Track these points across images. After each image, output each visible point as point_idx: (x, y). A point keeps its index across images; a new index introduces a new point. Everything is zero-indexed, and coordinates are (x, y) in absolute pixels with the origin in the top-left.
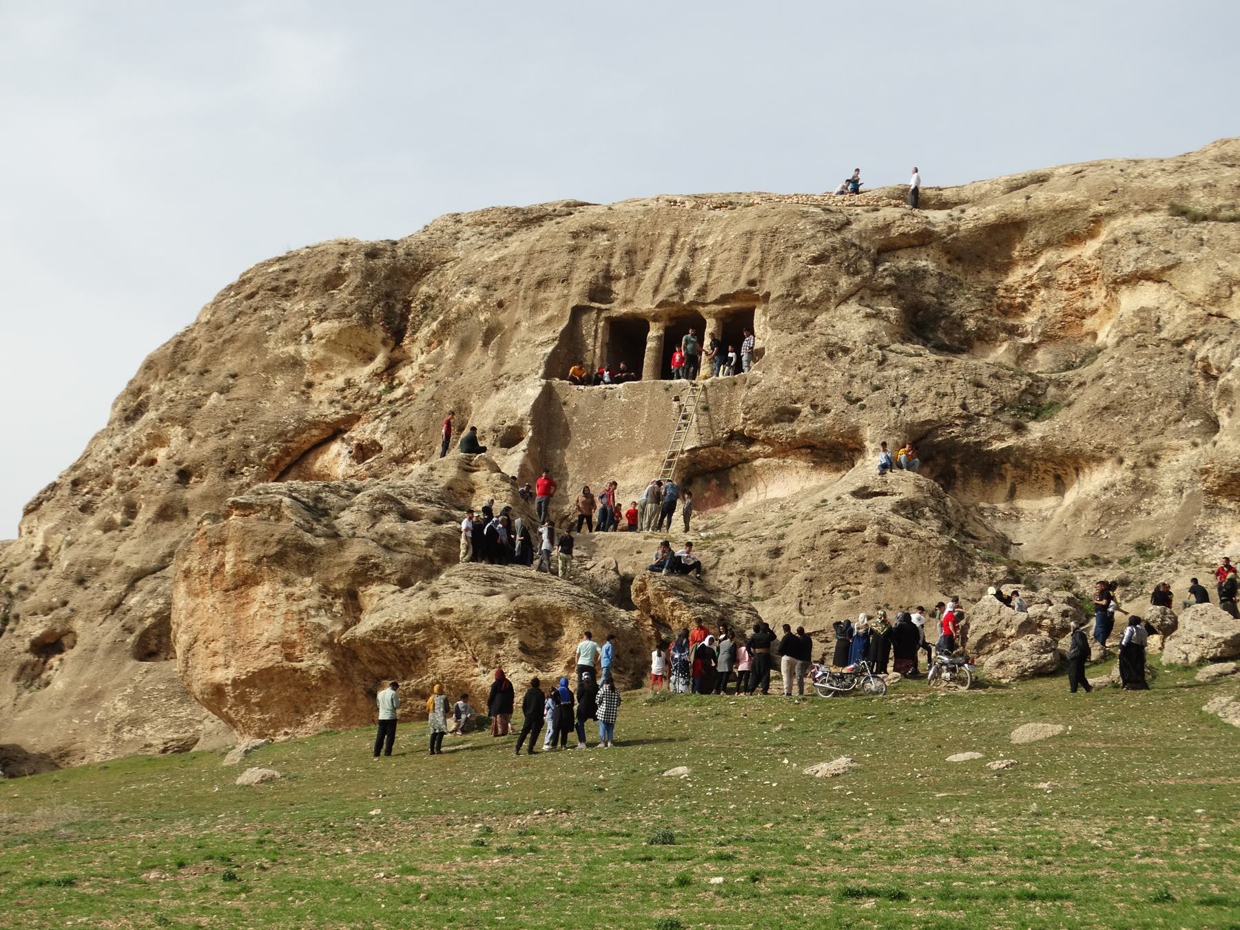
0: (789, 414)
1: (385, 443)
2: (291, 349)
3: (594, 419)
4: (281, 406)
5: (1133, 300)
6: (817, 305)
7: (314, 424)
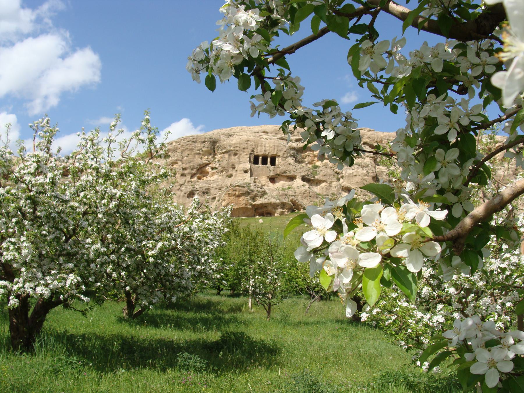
0: (285, 172)
6: (286, 157)
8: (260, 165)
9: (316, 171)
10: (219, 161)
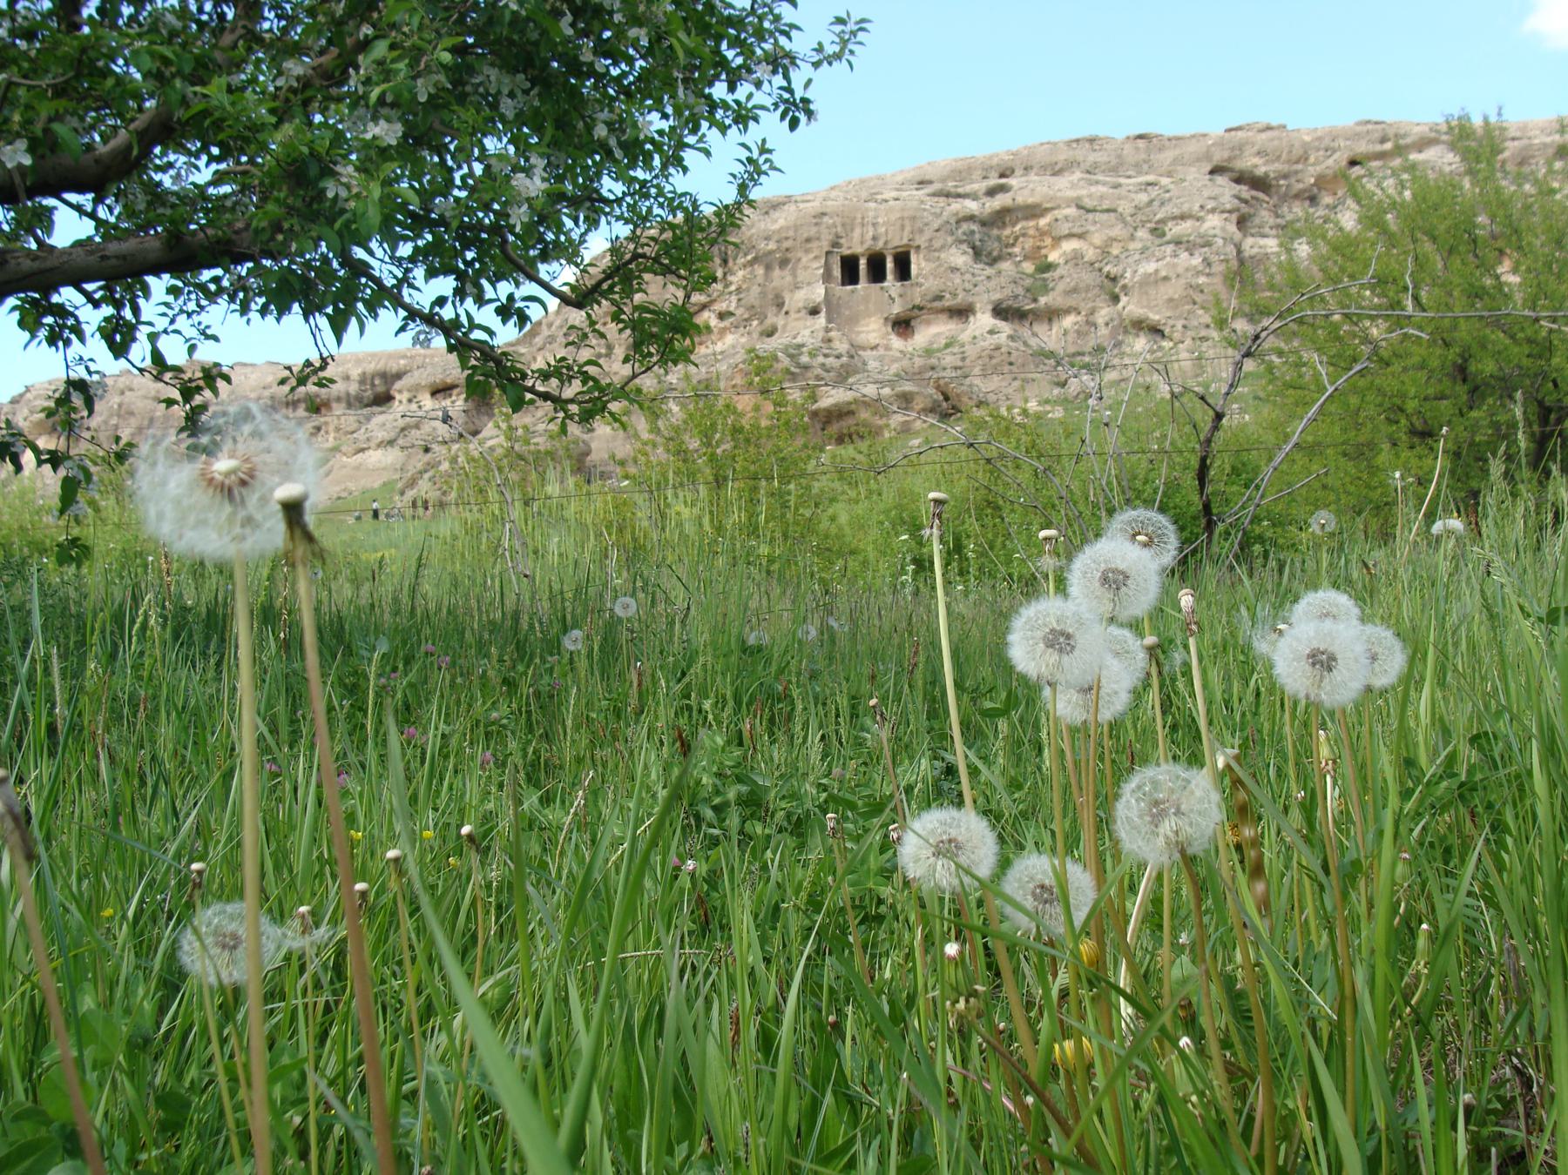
0: (939, 298)
1: (738, 312)
5: (1069, 246)
8: (863, 285)
9: (1045, 280)
10: (739, 290)
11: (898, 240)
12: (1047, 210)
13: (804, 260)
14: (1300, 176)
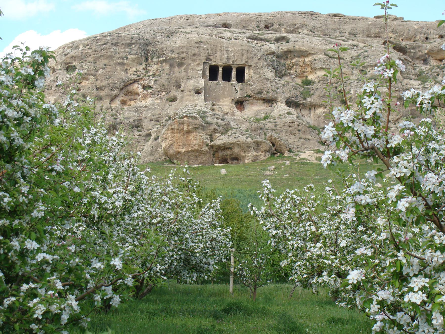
0: (260, 93)
1: (155, 87)
2: (122, 60)
3: (215, 89)
4: (121, 75)
5: (321, 73)
7: (131, 80)
8: (220, 81)
9: (308, 89)
11: (240, 61)
12: (310, 54)
13: (192, 65)
14: (420, 49)
